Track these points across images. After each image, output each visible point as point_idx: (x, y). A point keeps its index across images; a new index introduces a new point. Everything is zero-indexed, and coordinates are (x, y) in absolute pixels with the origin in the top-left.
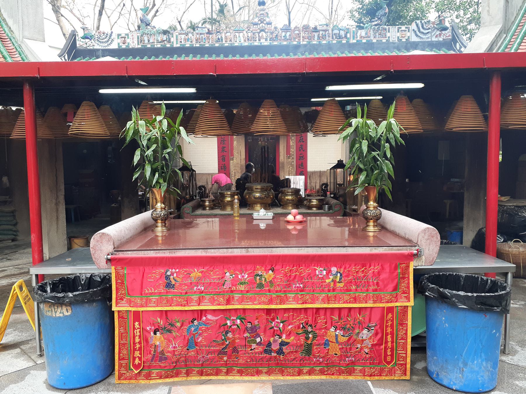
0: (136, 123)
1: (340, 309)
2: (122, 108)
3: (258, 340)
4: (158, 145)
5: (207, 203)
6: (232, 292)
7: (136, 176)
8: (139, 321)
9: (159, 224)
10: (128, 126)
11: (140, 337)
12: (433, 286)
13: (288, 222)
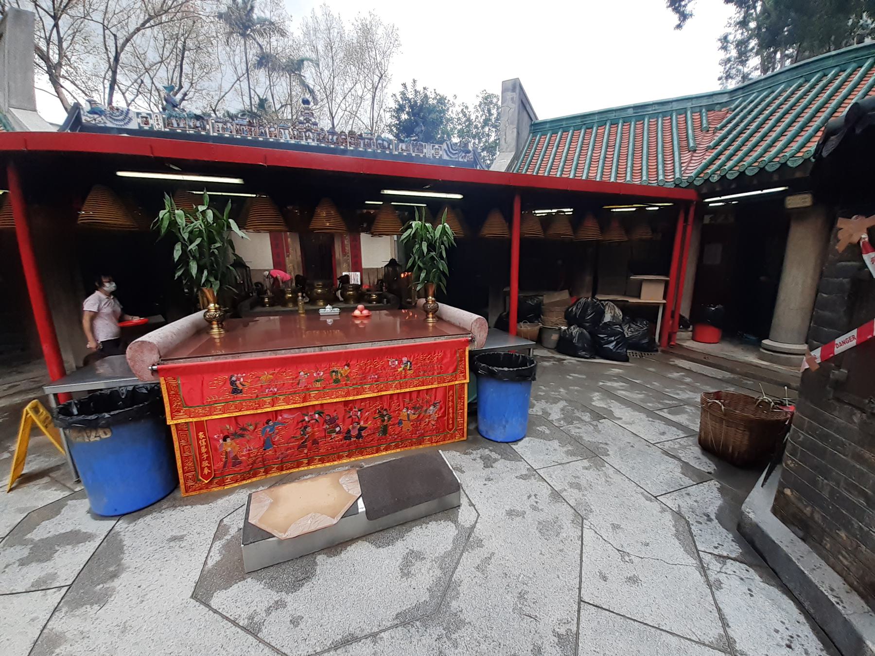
0: (172, 213)
1: (410, 392)
2: (151, 196)
3: (338, 429)
4: (203, 239)
5: (266, 300)
6: (308, 389)
7: (179, 273)
8: (203, 431)
9: (215, 326)
10: (161, 216)
11: (206, 446)
12: (484, 364)
13: (356, 317)
